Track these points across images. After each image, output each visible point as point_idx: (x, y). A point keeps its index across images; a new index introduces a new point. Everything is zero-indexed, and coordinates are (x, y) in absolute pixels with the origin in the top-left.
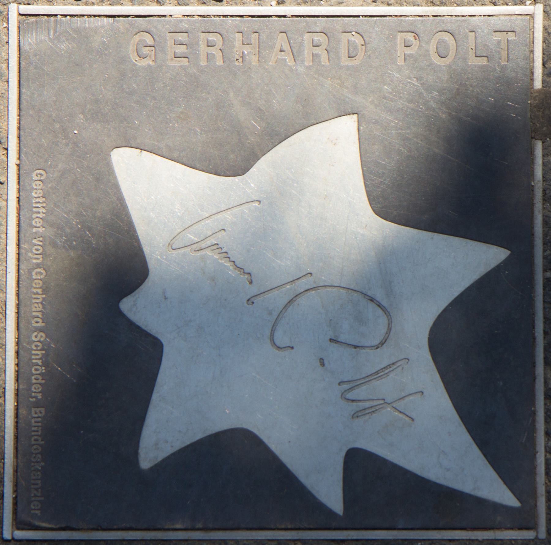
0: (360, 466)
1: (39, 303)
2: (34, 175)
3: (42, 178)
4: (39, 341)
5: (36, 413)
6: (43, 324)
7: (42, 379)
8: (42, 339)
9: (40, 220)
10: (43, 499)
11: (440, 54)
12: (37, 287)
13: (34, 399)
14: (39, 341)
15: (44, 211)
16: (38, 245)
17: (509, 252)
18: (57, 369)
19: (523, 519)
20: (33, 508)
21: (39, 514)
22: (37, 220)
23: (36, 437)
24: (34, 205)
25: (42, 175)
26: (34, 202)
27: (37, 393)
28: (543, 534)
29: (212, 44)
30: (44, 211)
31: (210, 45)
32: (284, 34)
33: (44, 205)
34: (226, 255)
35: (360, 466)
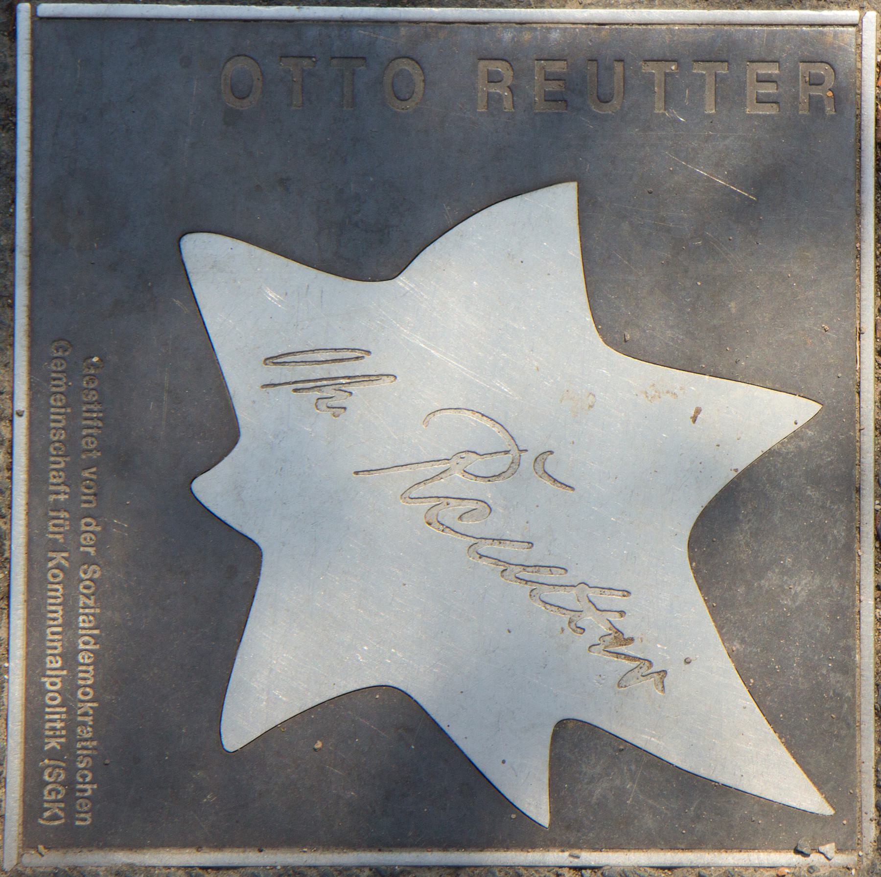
1: (59, 655)
4: (90, 580)
7: (95, 644)
8: (96, 576)
10: (98, 611)
12: (59, 369)
14: (90, 580)
15: (68, 490)
18: (119, 520)
19: (841, 829)
20: (84, 542)
23: (85, 591)
28: (24, 10)
29: (817, 82)
31: (494, 78)
34: (368, 378)
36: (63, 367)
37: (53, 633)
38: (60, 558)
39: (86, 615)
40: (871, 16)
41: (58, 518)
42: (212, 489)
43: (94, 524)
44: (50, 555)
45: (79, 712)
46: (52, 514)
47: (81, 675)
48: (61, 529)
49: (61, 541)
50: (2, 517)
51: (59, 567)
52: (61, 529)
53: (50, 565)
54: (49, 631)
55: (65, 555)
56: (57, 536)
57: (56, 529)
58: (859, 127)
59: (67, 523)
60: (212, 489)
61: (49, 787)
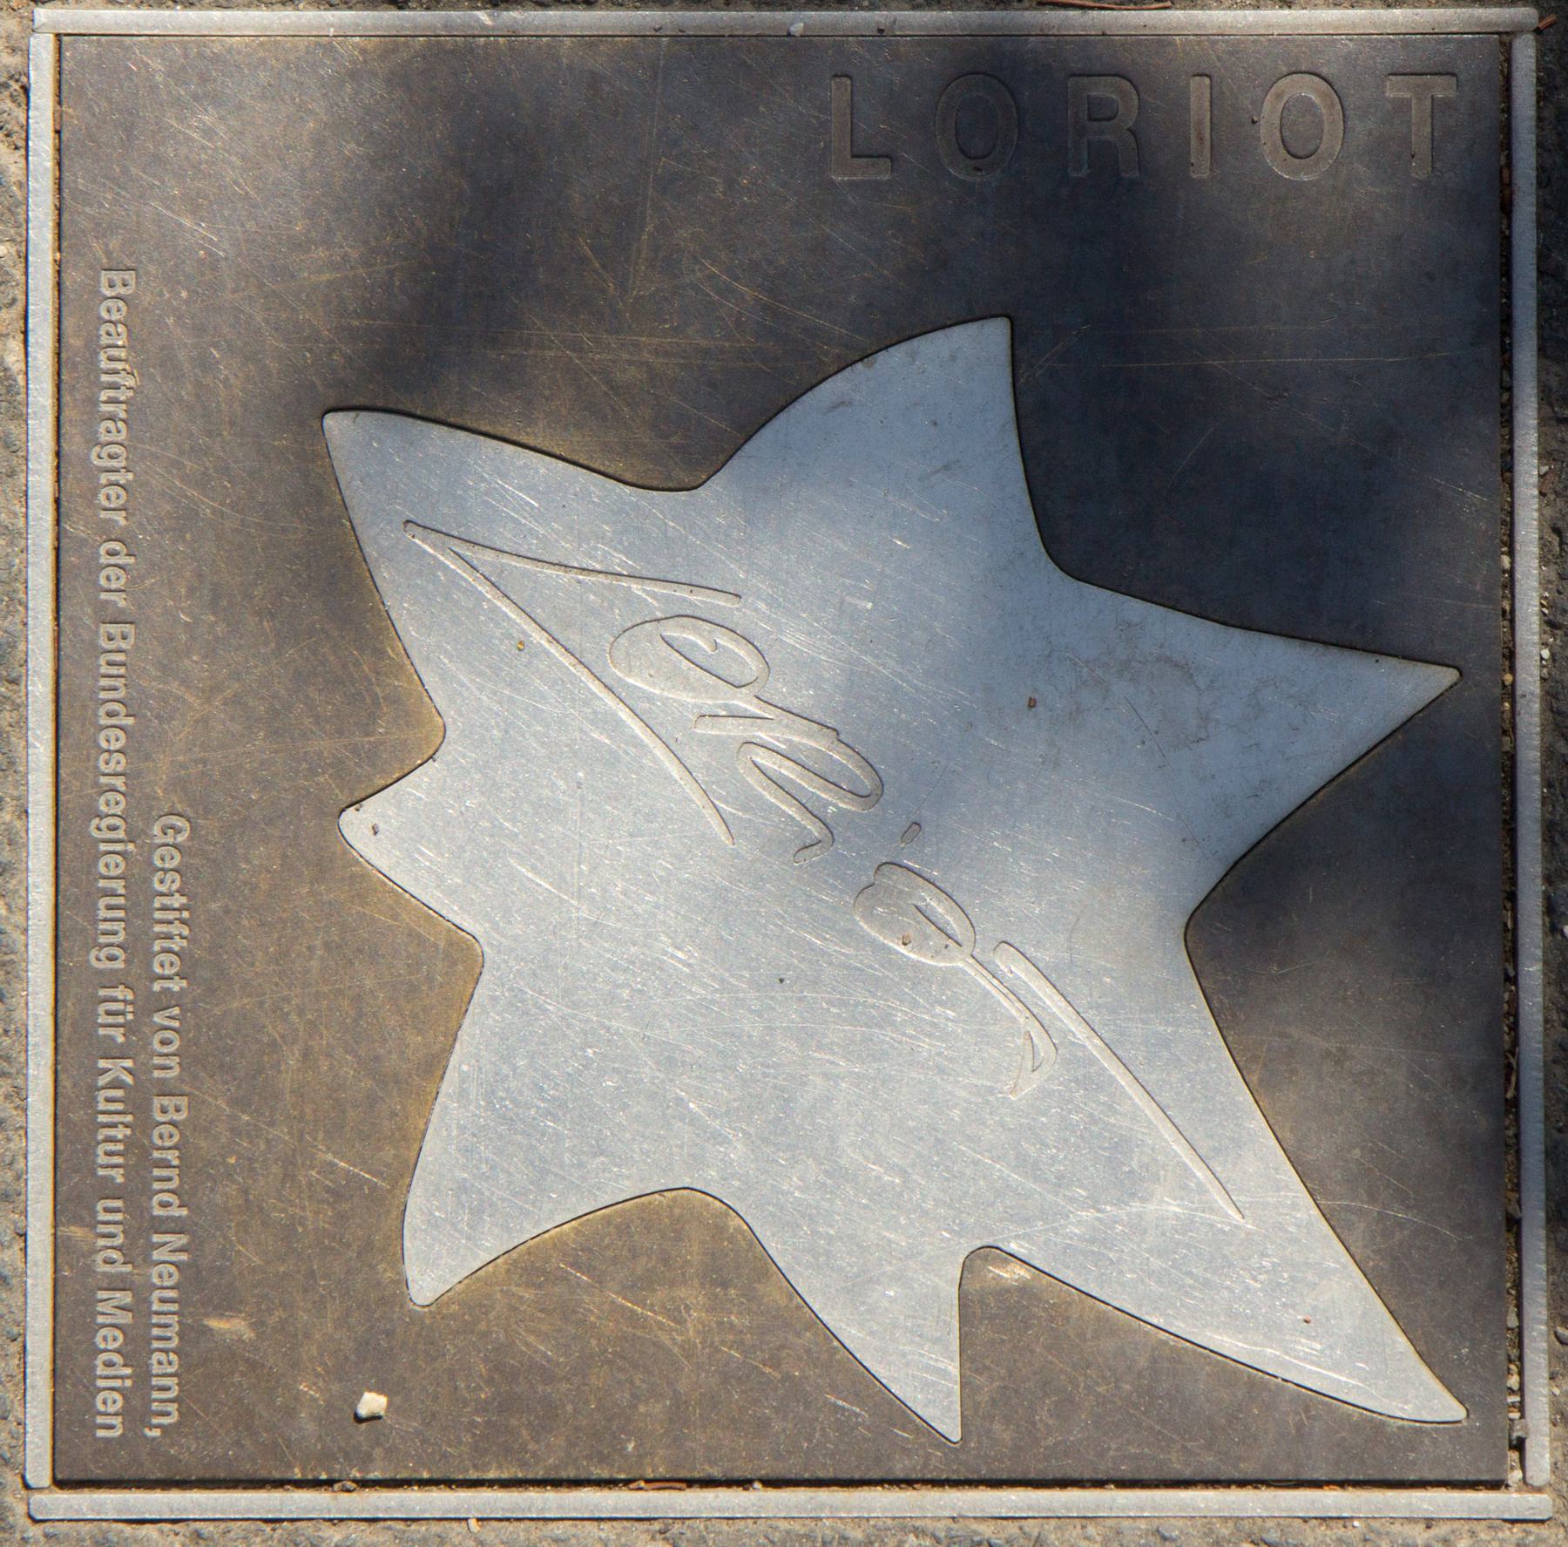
0: (1006, 1321)
2: (156, 830)
3: (180, 839)
4: (173, 1123)
5: (164, 1111)
6: (184, 1212)
9: (174, 958)
11: (1293, 151)
13: (156, 1433)
15: (186, 932)
16: (166, 1028)
17: (992, 337)
21: (120, 1180)
22: (112, 491)
23: (165, 1050)
24: (158, 915)
25: (178, 831)
26: (157, 905)
27: (167, 1055)
30: (186, 932)
32: (1207, 81)
33: (186, 914)
35: (1006, 1321)
36: (121, 501)
37: (109, 1154)
38: (118, 1069)
39: (166, 1351)
40: (42, 14)
41: (115, 1000)
42: (390, 835)
43: (177, 1202)
44: (102, 1064)
45: (102, 1081)
46: (102, 993)
47: (155, 1332)
48: (120, 1020)
49: (120, 1180)
50: (6, 1197)
51: (116, 1084)
52: (120, 1020)
53: (102, 1081)
54: (102, 1009)
55: (128, 1063)
56: (113, 1172)
57: (110, 1020)
58: (1511, 781)
59: (130, 1008)
60: (390, 835)
61: (104, 1357)
